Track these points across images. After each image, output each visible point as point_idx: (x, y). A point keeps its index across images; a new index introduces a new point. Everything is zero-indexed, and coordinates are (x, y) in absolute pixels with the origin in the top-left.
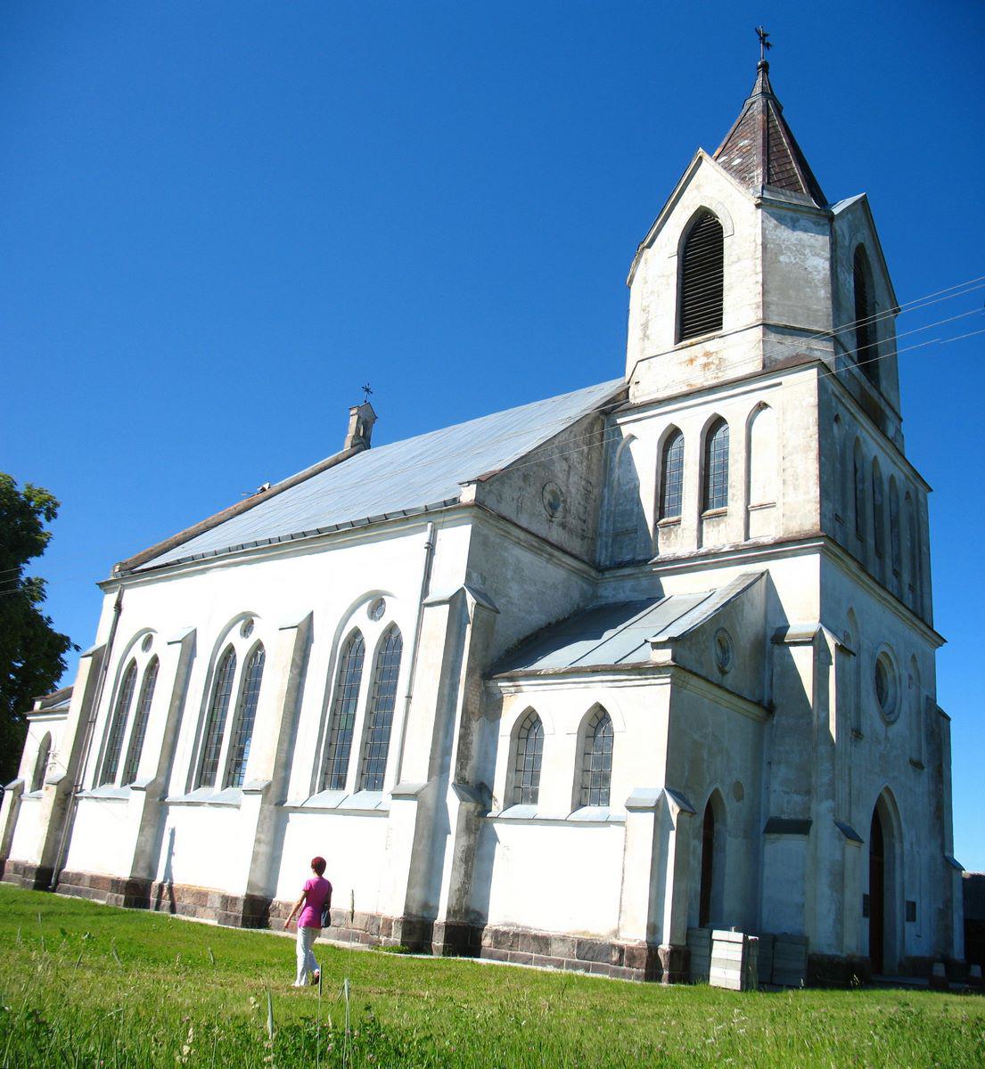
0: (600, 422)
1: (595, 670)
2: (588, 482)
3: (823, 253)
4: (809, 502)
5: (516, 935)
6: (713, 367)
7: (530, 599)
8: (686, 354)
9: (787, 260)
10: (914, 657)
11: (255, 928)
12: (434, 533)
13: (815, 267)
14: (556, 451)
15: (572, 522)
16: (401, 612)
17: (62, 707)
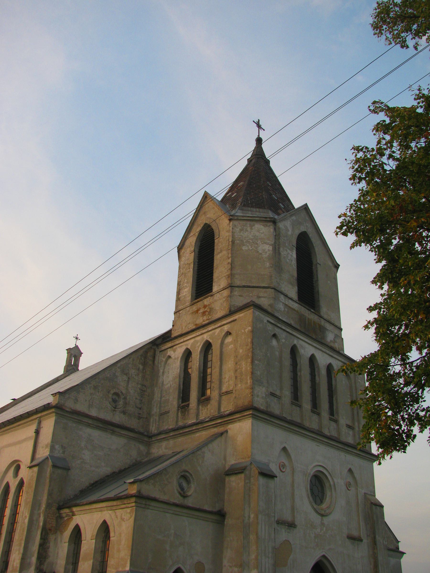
2: (143, 385)
3: (268, 241)
6: (207, 313)
8: (195, 308)
9: (247, 248)
10: (350, 470)
13: (264, 250)
14: (119, 370)
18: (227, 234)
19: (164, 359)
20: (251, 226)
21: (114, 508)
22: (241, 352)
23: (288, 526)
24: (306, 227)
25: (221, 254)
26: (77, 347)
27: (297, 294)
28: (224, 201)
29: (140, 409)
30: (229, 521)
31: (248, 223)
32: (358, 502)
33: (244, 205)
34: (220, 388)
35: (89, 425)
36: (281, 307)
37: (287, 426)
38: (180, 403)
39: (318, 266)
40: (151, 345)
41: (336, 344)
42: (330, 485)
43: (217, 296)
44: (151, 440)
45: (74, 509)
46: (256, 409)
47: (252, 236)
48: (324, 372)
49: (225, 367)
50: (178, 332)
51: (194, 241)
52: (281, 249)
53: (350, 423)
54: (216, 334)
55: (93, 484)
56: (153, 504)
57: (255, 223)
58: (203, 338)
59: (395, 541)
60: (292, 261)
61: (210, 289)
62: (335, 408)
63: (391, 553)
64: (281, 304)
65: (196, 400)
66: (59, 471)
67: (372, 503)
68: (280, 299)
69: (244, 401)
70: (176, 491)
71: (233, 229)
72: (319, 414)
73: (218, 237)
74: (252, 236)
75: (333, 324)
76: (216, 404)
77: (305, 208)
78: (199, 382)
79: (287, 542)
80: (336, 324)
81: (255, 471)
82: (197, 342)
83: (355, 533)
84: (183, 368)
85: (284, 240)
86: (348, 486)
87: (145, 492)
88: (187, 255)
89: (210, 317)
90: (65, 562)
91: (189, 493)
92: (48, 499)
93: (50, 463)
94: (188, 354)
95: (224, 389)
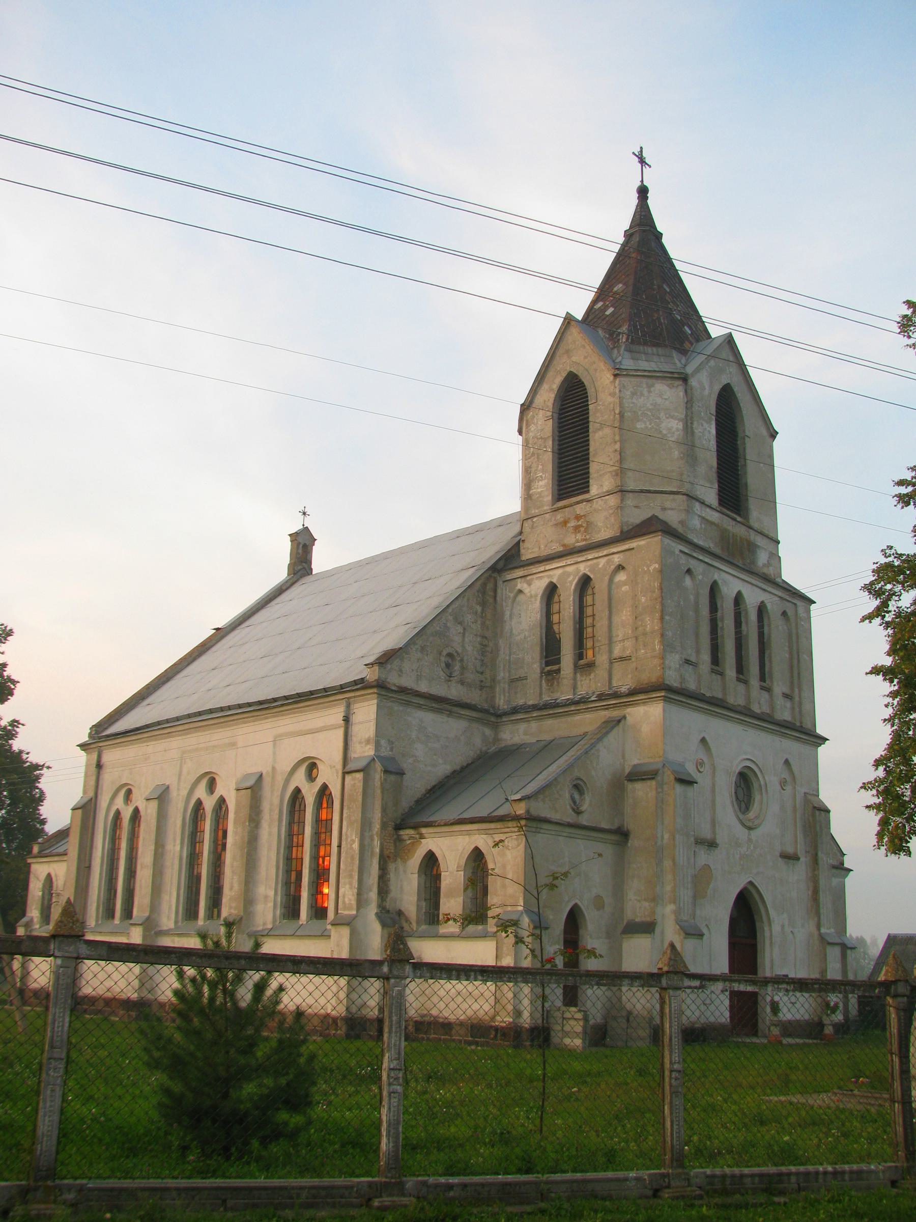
0: (492, 580)
1: (473, 821)
2: (483, 637)
4: (654, 657)
5: (429, 1023)
6: (582, 529)
7: (435, 755)
8: (559, 517)
9: (643, 426)
10: (787, 762)
11: (746, 974)
12: (348, 706)
13: (669, 429)
15: (470, 676)
16: (329, 775)
17: (56, 851)
18: (610, 399)
19: (512, 595)
20: (649, 387)
21: (491, 832)
22: (643, 600)
23: (708, 846)
24: (730, 376)
25: (600, 433)
26: (306, 530)
27: (717, 497)
28: (590, 318)
29: (482, 673)
30: (633, 842)
31: (644, 380)
32: (795, 807)
33: (633, 342)
34: (610, 651)
35: (419, 707)
36: (696, 523)
37: (706, 707)
38: (544, 666)
39: (746, 438)
40: (490, 572)
41: (771, 568)
42: (760, 786)
43: (598, 504)
44: (499, 721)
45: (424, 830)
46: (669, 689)
47: (651, 404)
48: (753, 616)
49: (616, 619)
50: (533, 552)
51: (552, 400)
52: (695, 424)
53: (787, 691)
54: (600, 566)
55: (431, 790)
56: (546, 826)
57: (654, 381)
58: (578, 570)
59: (839, 854)
60: (710, 441)
61: (584, 487)
62: (767, 669)
63: (834, 871)
64: (697, 517)
65: (572, 666)
66: (392, 778)
67: (814, 807)
68: (695, 509)
69: (650, 673)
70: (568, 807)
71: (620, 391)
72: (745, 682)
73: (593, 401)
74: (651, 404)
75: (767, 537)
76: (606, 675)
77: (729, 341)
78: (575, 635)
79: (707, 867)
80: (772, 535)
81: (669, 777)
82: (569, 574)
83: (790, 850)
84: (544, 610)
85: (699, 406)
86: (783, 783)
87: (534, 812)
88: (540, 423)
89: (588, 537)
90: (416, 898)
91: (583, 808)
92: (382, 817)
93: (378, 766)
94: (552, 590)
95: (617, 651)
